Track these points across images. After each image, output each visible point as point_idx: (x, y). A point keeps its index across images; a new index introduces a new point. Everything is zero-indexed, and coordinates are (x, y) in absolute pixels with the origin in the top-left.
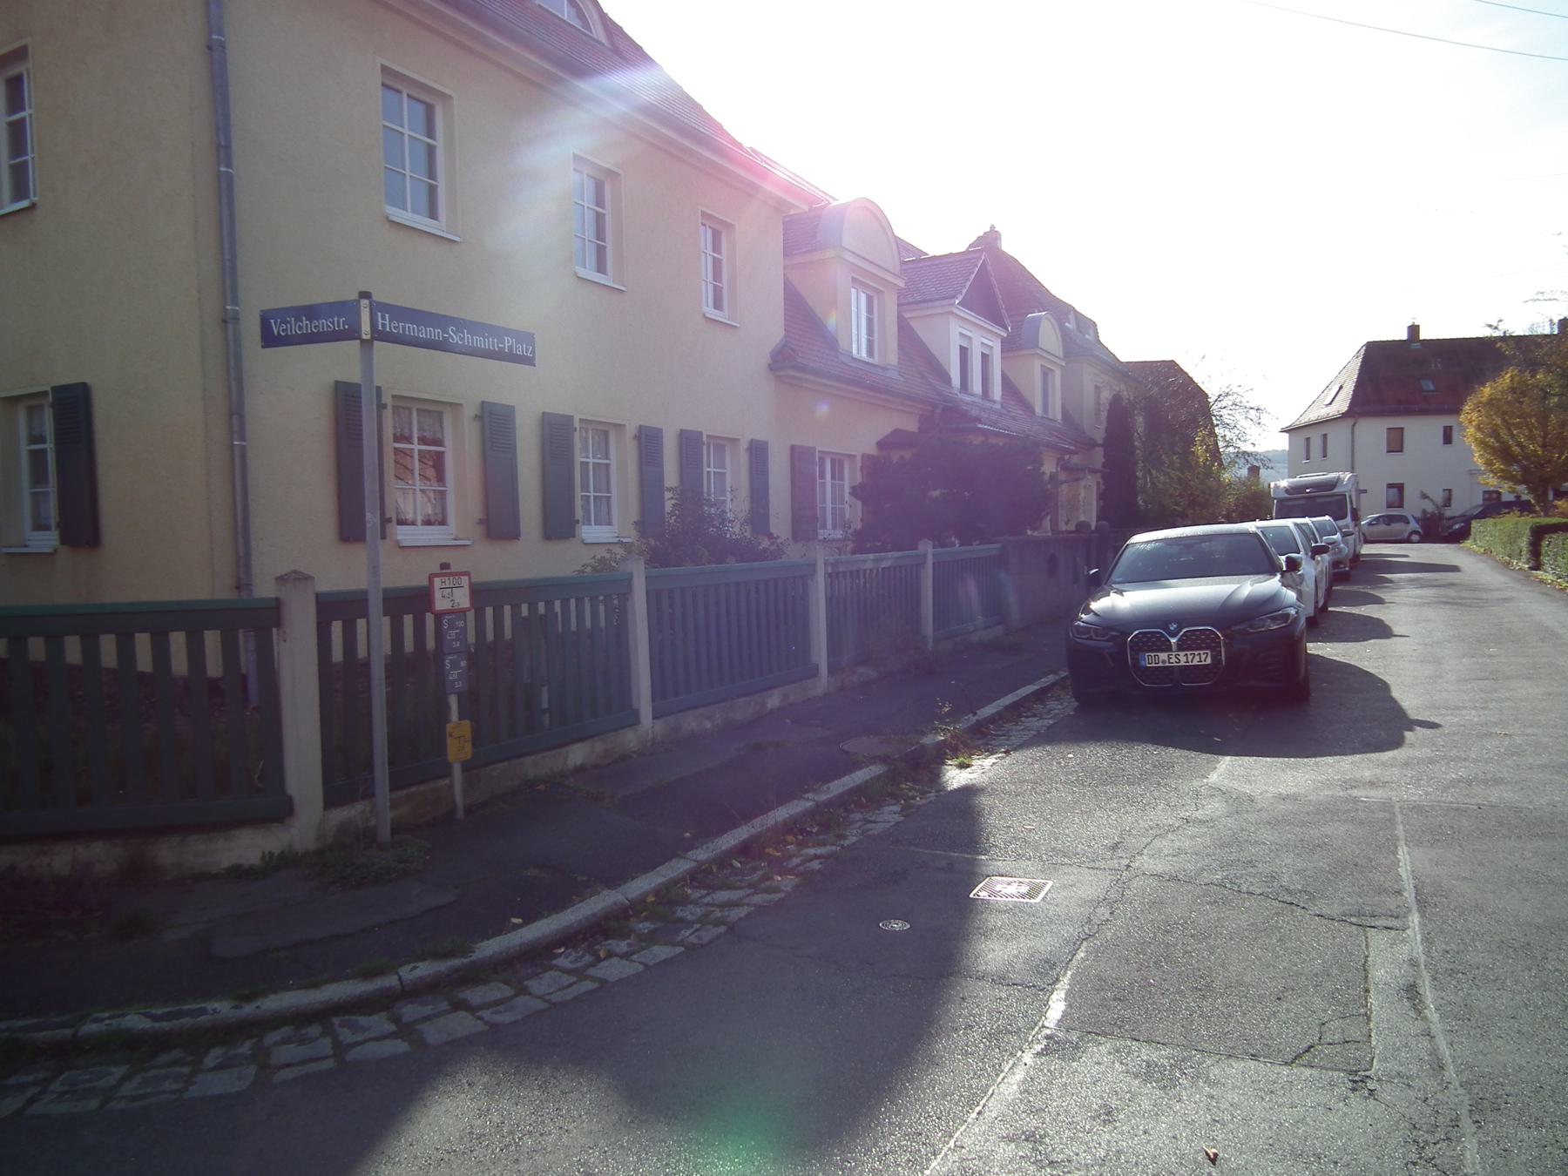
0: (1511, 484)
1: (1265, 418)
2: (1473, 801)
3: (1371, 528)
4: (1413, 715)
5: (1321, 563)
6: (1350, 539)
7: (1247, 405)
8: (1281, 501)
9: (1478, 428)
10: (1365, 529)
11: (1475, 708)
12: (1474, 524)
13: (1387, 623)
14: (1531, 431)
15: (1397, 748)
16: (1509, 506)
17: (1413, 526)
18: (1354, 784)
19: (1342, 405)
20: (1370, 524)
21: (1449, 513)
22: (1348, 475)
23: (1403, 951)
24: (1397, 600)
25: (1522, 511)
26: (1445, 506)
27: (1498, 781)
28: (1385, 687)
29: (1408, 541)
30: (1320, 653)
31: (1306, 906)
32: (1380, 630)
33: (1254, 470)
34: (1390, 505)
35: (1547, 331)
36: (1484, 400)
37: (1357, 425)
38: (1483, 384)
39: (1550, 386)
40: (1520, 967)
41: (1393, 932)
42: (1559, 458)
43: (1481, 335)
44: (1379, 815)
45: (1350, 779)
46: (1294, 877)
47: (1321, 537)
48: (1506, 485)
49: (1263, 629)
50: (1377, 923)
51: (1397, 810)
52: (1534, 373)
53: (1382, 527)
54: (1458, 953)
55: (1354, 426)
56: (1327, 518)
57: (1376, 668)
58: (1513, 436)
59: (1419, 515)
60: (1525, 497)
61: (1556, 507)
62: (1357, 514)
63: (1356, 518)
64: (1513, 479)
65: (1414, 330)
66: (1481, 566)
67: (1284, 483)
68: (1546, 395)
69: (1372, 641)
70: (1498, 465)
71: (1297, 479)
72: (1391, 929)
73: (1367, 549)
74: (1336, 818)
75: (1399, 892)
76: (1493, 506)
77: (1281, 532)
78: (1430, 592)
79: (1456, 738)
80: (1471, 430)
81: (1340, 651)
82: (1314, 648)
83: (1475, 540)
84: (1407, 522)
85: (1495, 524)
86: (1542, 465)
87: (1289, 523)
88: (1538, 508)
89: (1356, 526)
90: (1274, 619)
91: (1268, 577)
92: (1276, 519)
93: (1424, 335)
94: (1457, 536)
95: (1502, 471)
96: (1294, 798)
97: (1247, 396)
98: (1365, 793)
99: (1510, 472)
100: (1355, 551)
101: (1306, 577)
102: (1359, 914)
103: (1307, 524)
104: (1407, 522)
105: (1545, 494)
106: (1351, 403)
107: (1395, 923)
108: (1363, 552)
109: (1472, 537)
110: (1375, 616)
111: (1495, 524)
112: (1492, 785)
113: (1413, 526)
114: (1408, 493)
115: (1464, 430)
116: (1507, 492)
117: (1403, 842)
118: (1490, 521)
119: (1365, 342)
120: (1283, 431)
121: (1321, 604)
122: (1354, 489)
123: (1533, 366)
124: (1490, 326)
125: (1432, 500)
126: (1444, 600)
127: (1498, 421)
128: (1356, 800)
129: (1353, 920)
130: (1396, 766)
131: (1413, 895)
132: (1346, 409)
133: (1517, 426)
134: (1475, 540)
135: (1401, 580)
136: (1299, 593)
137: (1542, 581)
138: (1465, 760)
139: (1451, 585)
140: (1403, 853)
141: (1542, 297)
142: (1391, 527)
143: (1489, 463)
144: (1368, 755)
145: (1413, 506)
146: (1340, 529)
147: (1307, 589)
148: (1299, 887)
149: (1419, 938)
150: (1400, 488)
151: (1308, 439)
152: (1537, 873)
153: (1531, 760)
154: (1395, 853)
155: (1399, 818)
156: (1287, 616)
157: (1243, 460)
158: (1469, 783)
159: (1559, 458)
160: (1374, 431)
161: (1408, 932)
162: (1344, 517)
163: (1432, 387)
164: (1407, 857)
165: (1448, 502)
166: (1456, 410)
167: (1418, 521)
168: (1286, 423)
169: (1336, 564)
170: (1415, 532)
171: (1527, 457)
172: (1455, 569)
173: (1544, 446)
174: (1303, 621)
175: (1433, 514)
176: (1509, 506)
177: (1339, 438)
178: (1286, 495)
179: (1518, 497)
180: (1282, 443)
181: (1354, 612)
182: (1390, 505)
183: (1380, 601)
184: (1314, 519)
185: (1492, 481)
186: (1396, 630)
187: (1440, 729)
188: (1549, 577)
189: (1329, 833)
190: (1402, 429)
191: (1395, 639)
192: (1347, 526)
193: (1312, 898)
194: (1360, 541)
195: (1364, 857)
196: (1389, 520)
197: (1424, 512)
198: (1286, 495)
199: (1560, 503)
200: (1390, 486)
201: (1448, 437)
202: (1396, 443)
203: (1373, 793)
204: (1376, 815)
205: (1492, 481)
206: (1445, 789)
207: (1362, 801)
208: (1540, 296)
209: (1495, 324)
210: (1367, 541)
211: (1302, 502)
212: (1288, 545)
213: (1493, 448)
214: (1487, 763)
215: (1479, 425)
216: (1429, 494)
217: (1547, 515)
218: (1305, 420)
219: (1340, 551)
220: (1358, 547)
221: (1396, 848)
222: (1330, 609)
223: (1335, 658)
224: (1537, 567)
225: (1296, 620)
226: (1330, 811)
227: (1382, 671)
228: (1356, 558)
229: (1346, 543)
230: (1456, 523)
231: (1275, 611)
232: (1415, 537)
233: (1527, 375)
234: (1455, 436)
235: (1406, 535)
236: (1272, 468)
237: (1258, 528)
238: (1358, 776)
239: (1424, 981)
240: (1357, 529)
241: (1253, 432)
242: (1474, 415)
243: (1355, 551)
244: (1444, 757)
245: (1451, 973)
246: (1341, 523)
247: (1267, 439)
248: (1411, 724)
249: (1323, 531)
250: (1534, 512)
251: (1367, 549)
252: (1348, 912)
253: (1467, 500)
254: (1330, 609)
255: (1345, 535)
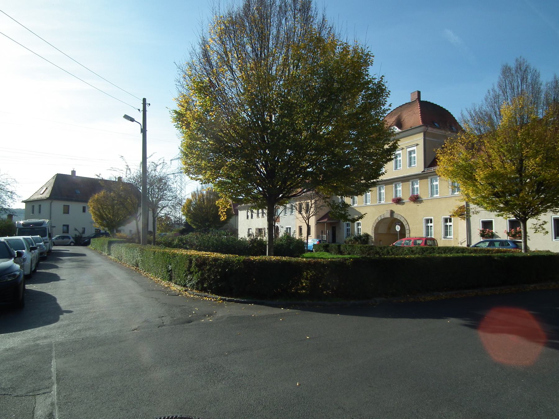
0: (103, 227)
1: (15, 196)
2: (81, 337)
3: (57, 240)
4: (64, 309)
5: (34, 254)
6: (48, 244)
7: (7, 190)
8: (20, 229)
9: (93, 208)
10: (54, 241)
11: (85, 304)
12: (92, 240)
13: (58, 275)
14: (109, 211)
15: (56, 322)
16: (103, 234)
17: (72, 240)
18: (38, 338)
19: (47, 195)
20: (56, 239)
21: (84, 236)
22: (47, 221)
23: (49, 401)
24: (63, 266)
25: (106, 236)
26: (83, 233)
27: (90, 329)
28: (55, 299)
29: (70, 245)
30: (31, 288)
31: (11, 394)
32: (55, 278)
33: (10, 216)
34: (64, 232)
35: (114, 180)
36: (95, 199)
37: (52, 203)
38: (95, 194)
39: (115, 197)
40: (89, 394)
41: (46, 394)
42: (117, 220)
43: (93, 177)
44: (46, 349)
45: (37, 337)
46: (7, 383)
47: (35, 243)
48: (102, 228)
49: (5, 281)
50: (40, 392)
51: (53, 345)
52: (110, 192)
53: (60, 240)
54: (69, 395)
55: (51, 203)
56: (38, 236)
57: (52, 292)
58: (104, 211)
59: (74, 236)
60: (108, 232)
61: (116, 235)
62: (51, 235)
63: (50, 236)
64: (104, 225)
65: (73, 172)
66: (93, 254)
67: (22, 222)
68: (114, 200)
69: (52, 282)
70: (99, 221)
71: (27, 221)
72: (46, 393)
73: (54, 248)
74: (29, 354)
75: (50, 378)
76: (98, 234)
77: (18, 242)
78: (74, 263)
79: (78, 315)
80: (91, 208)
81: (39, 287)
82: (28, 287)
83: (92, 245)
84: (70, 239)
85: (98, 240)
86: (112, 222)
87: (21, 237)
88: (111, 235)
89: (50, 239)
90: (9, 276)
91: (9, 259)
92: (18, 236)
93: (77, 174)
94: (86, 243)
95: (100, 223)
96: (12, 349)
97: (8, 187)
98: (42, 341)
99: (103, 223)
100: (49, 248)
101: (27, 259)
102: (34, 391)
103: (30, 238)
104: (70, 239)
105: (113, 231)
106: (50, 195)
107: (48, 390)
108: (53, 249)
109: (91, 244)
110: (54, 273)
111: (98, 240)
112: (88, 330)
113: (72, 240)
114: (71, 229)
115: (89, 208)
116: (102, 229)
117: (54, 358)
118: (96, 239)
119: (56, 174)
120: (23, 202)
121: (33, 269)
122: (50, 226)
123: (110, 190)
124: (97, 175)
125: (78, 231)
126: (79, 266)
127: (100, 206)
128: (38, 345)
129: (31, 394)
130: (55, 329)
131: (56, 377)
132: (48, 196)
133: (105, 209)
134: (92, 245)
135: (66, 259)
136: (22, 267)
137: (111, 259)
138: (80, 323)
139: (82, 261)
140: (54, 363)
141: (112, 169)
142: (64, 241)
143: (96, 220)
144: (45, 326)
145: (72, 233)
146: (44, 240)
147: (27, 264)
148: (9, 386)
149: (56, 393)
150: (68, 226)
151: (33, 206)
152: (98, 358)
153: (101, 319)
154: (51, 363)
155: (54, 349)
156: (15, 275)
157: (4, 212)
158: (80, 331)
159: (117, 220)
160: (59, 206)
161: (52, 392)
162: (46, 236)
163: (79, 193)
164: (55, 363)
165: (84, 232)
166: (86, 201)
167: (73, 238)
168: (25, 199)
169: (41, 254)
170: (72, 242)
171: (108, 219)
172: (84, 255)
173: (113, 216)
174: (22, 276)
175: (79, 236)
176: (103, 234)
177: (45, 207)
178: (23, 227)
179: (106, 231)
180: (23, 206)
181: (47, 272)
182: (64, 232)
183: (57, 267)
184: (32, 236)
185: (97, 226)
186: (61, 278)
187: (73, 313)
188: (113, 258)
189: (25, 360)
190: (69, 206)
191: (60, 281)
192: (46, 239)
193: (14, 389)
194: (51, 245)
195: (38, 367)
196: (63, 237)
197: (76, 235)
198: (23, 227)
199: (117, 234)
200: (64, 225)
201: (84, 210)
202: (66, 210)
203: (45, 341)
204: (45, 349)
205: (97, 226)
206: (72, 334)
207: (41, 345)
208: (112, 169)
209: (99, 175)
210: (55, 245)
211: (29, 230)
212: (18, 245)
213: (98, 215)
214: (87, 322)
215: (94, 207)
216: (78, 229)
217: (113, 238)
218: (32, 199)
219: (43, 248)
220: (51, 247)
221: (51, 360)
222: (37, 271)
223: (37, 290)
224: (109, 255)
225: (19, 276)
226: (26, 351)
227: (54, 293)
228: (50, 252)
229: (46, 246)
230: (86, 239)
231: (10, 273)
232: (72, 244)
233: (108, 193)
234: (87, 210)
235: (69, 243)
236: (17, 216)
237: (5, 240)
238: (40, 335)
239: (56, 410)
240: (50, 240)
241: (9, 201)
242: (92, 204)
243: (49, 248)
244: (72, 323)
245: (66, 404)
246: (44, 238)
247: (18, 205)
248: (62, 312)
249: (36, 241)
250: (110, 236)
251: (54, 248)
252: (28, 391)
253: (89, 232)
254: (37, 271)
255: (45, 243)
